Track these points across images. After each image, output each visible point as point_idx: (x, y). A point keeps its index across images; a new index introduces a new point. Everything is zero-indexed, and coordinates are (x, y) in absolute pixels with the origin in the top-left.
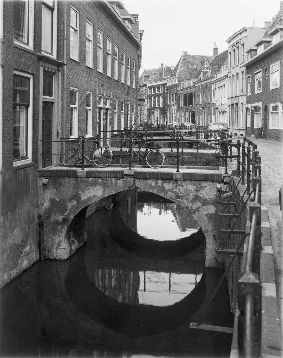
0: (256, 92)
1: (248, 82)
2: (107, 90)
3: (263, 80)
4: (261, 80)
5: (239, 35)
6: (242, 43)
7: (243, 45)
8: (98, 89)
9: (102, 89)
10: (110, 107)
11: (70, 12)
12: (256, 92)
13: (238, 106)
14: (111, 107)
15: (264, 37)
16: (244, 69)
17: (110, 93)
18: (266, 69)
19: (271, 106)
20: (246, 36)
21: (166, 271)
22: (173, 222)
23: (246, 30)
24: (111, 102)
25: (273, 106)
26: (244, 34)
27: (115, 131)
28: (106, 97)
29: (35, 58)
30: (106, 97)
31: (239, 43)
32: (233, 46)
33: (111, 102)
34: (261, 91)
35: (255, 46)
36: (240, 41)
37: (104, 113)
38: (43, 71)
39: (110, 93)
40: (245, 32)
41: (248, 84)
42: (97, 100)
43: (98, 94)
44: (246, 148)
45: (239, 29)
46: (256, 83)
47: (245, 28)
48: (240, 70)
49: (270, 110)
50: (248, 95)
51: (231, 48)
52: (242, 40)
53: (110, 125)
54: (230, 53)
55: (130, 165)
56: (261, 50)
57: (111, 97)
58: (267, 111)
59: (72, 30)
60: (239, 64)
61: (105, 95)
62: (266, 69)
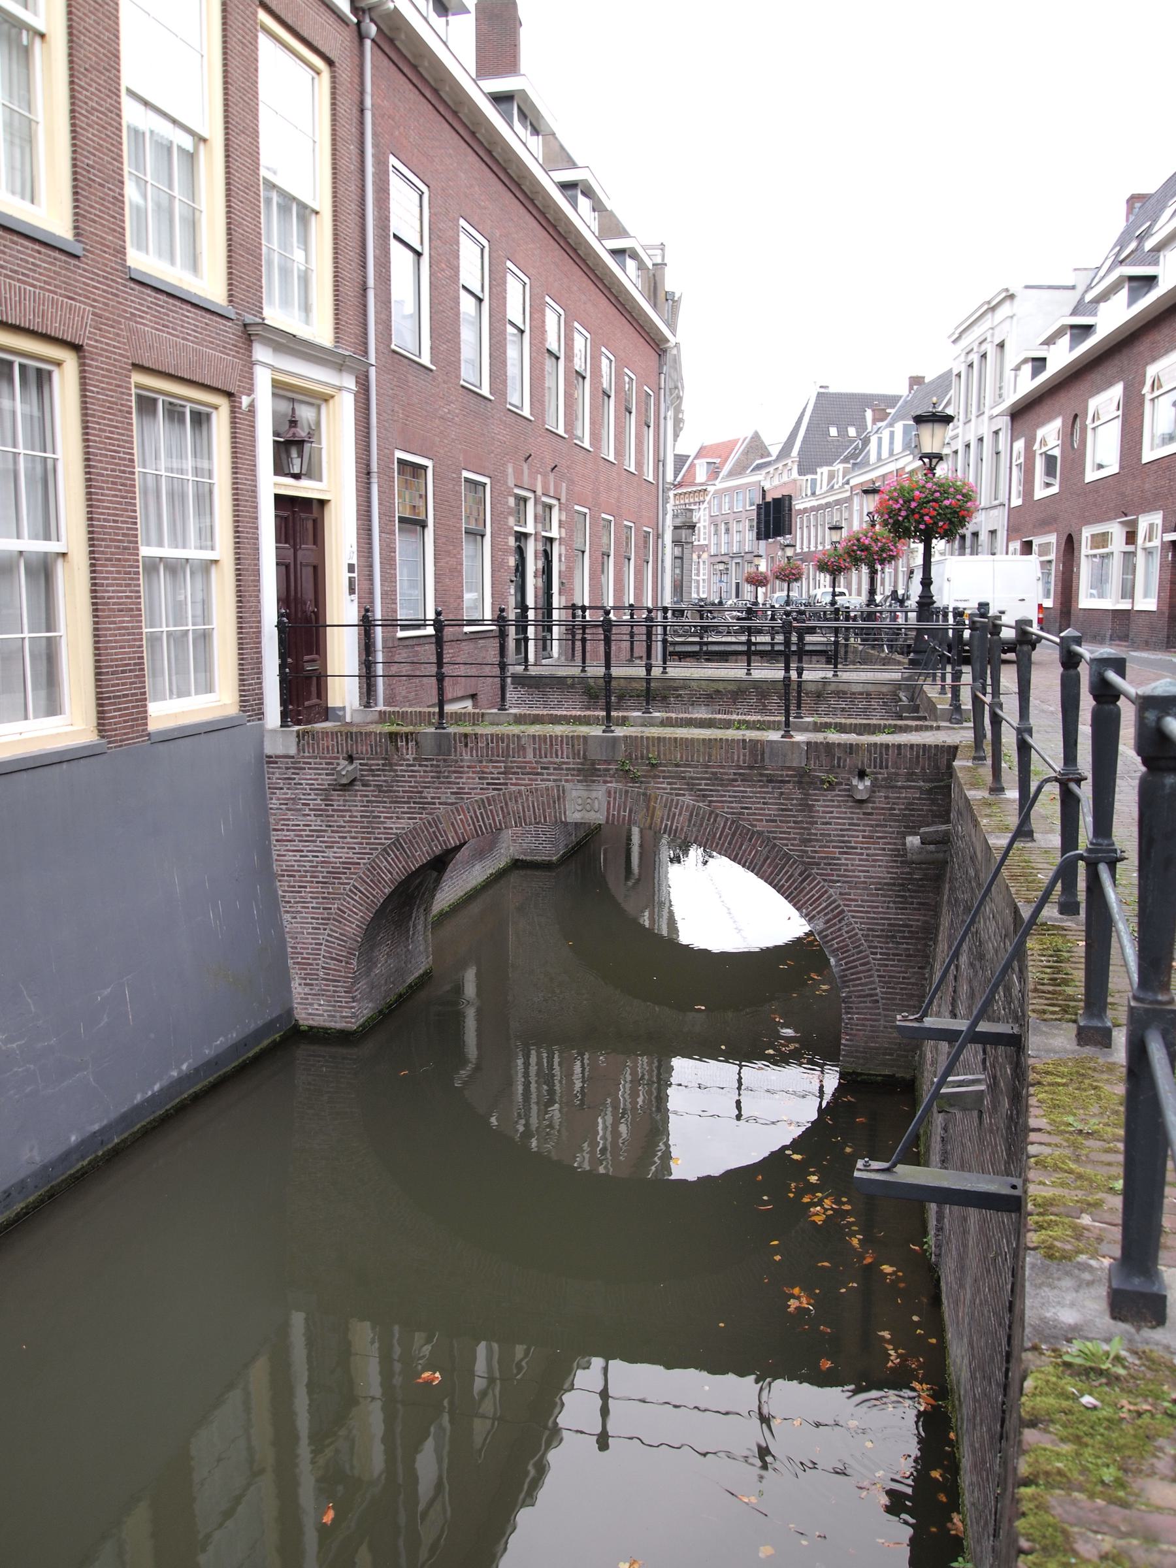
0: (1040, 493)
1: (1014, 463)
2: (545, 476)
3: (1062, 452)
4: (1057, 452)
5: (989, 315)
6: (997, 341)
7: (1001, 345)
8: (510, 470)
9: (526, 471)
10: (560, 533)
11: (573, 340)
12: (1040, 493)
13: (980, 543)
14: (563, 535)
15: (1074, 313)
16: (1004, 422)
17: (557, 487)
18: (1076, 416)
19: (1088, 535)
20: (1012, 317)
21: (728, 1057)
22: (1039, 580)
23: (1011, 297)
24: (563, 518)
25: (1093, 536)
26: (1005, 310)
27: (801, 639)
28: (544, 499)
29: (230, 332)
30: (544, 499)
31: (989, 340)
32: (968, 353)
33: (563, 518)
34: (1055, 490)
35: (1041, 344)
36: (993, 335)
37: (536, 552)
38: (273, 386)
39: (557, 487)
40: (1007, 304)
41: (1014, 469)
42: (509, 507)
43: (511, 483)
44: (1122, 703)
45: (990, 292)
46: (1040, 465)
47: (1007, 290)
48: (989, 427)
49: (1085, 549)
50: (1012, 505)
51: (962, 358)
52: (997, 331)
53: (560, 594)
54: (959, 375)
55: (608, 717)
56: (1061, 357)
57: (563, 501)
58: (1073, 552)
59: (510, 330)
60: (986, 410)
61: (539, 492)
62: (1076, 416)
